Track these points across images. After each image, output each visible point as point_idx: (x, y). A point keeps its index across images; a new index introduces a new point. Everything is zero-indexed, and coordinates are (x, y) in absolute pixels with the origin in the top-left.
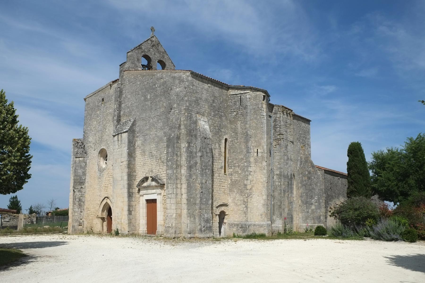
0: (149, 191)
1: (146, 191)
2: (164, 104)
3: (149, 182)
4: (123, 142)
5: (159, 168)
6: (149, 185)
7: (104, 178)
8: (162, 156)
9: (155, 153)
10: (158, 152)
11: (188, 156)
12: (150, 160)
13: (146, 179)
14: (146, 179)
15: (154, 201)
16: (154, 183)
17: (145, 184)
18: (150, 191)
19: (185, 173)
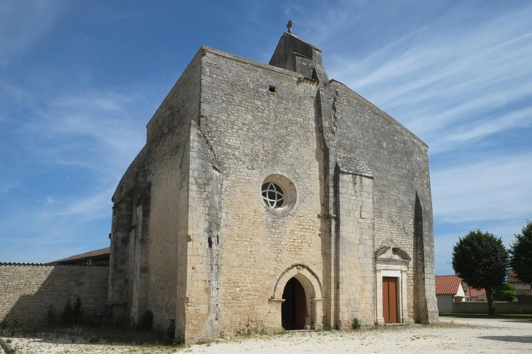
0: (390, 266)
1: (385, 265)
2: (407, 166)
3: (389, 254)
4: (365, 189)
5: (401, 239)
6: (389, 257)
7: (289, 230)
8: (405, 226)
9: (396, 219)
10: (401, 219)
11: (84, 339)
12: (388, 226)
13: (384, 249)
14: (384, 249)
15: (395, 280)
16: (396, 257)
17: (383, 256)
18: (391, 266)
19: (412, 266)
